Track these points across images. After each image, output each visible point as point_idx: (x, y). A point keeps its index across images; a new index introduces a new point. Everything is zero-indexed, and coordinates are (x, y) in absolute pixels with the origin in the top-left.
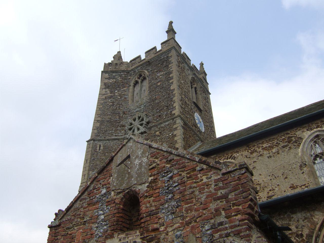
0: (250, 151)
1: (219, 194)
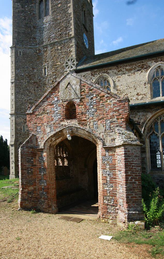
0: (118, 70)
1: (115, 109)
